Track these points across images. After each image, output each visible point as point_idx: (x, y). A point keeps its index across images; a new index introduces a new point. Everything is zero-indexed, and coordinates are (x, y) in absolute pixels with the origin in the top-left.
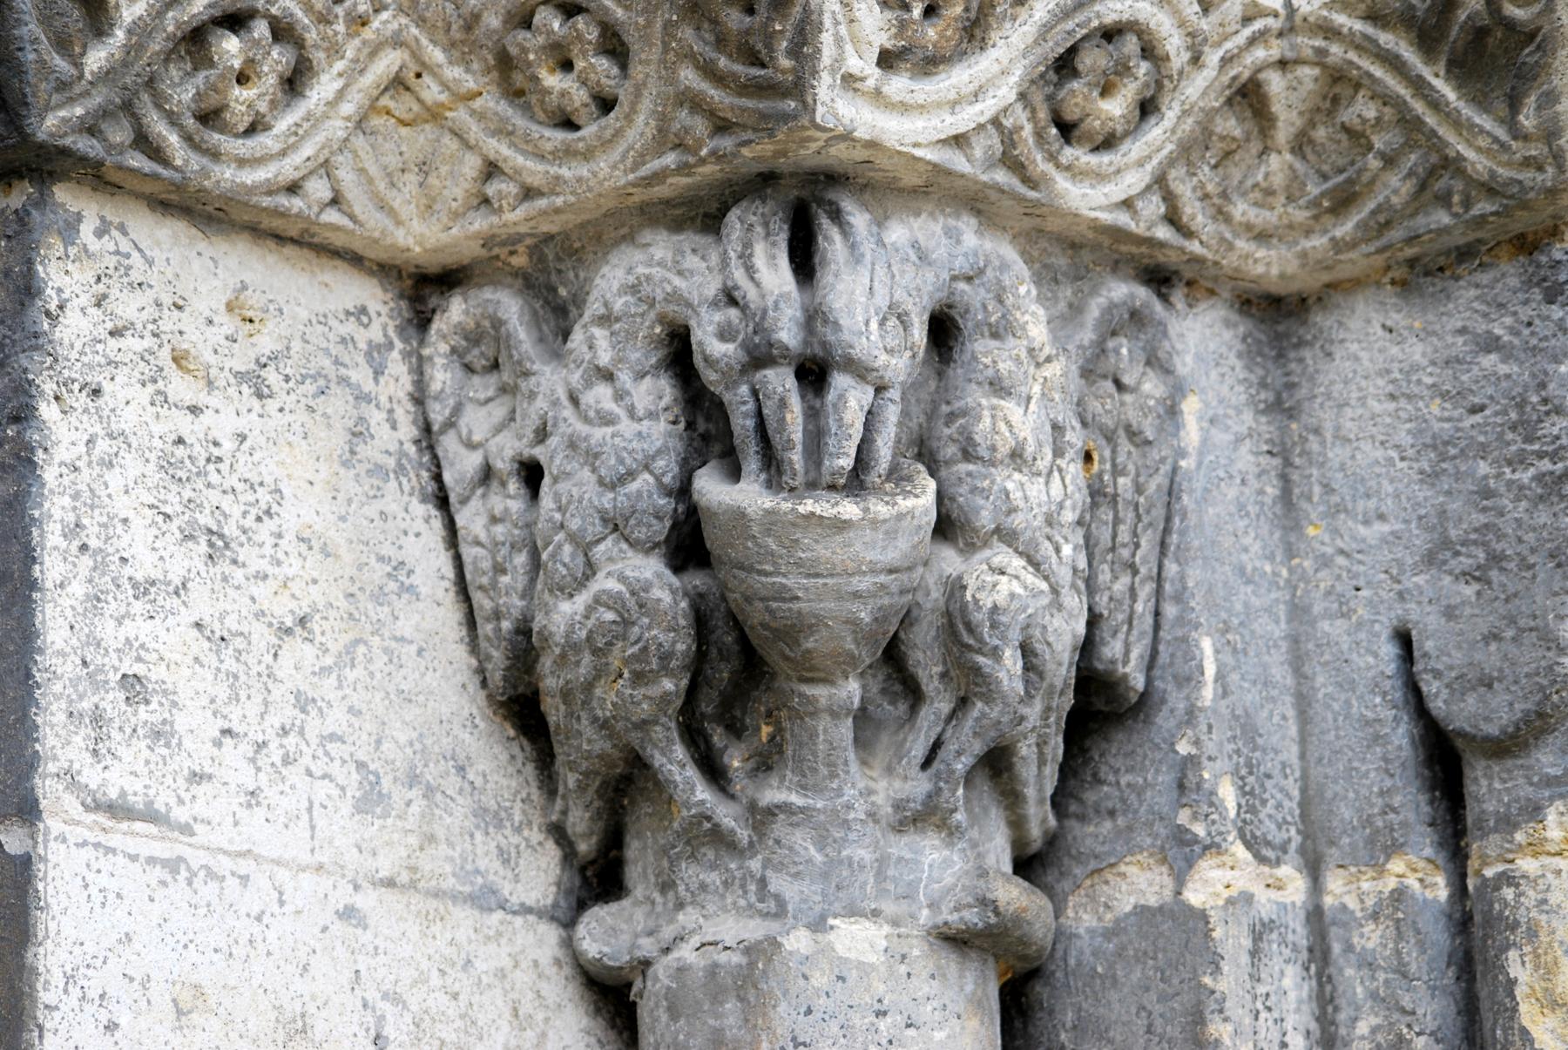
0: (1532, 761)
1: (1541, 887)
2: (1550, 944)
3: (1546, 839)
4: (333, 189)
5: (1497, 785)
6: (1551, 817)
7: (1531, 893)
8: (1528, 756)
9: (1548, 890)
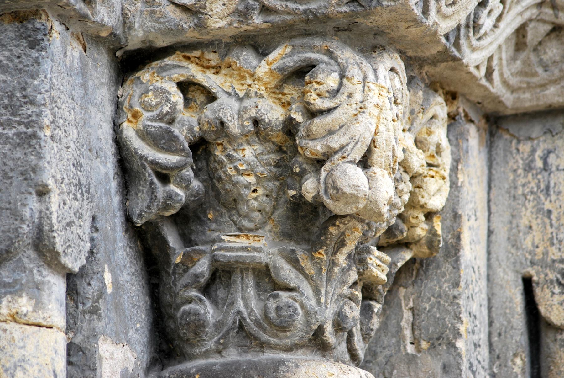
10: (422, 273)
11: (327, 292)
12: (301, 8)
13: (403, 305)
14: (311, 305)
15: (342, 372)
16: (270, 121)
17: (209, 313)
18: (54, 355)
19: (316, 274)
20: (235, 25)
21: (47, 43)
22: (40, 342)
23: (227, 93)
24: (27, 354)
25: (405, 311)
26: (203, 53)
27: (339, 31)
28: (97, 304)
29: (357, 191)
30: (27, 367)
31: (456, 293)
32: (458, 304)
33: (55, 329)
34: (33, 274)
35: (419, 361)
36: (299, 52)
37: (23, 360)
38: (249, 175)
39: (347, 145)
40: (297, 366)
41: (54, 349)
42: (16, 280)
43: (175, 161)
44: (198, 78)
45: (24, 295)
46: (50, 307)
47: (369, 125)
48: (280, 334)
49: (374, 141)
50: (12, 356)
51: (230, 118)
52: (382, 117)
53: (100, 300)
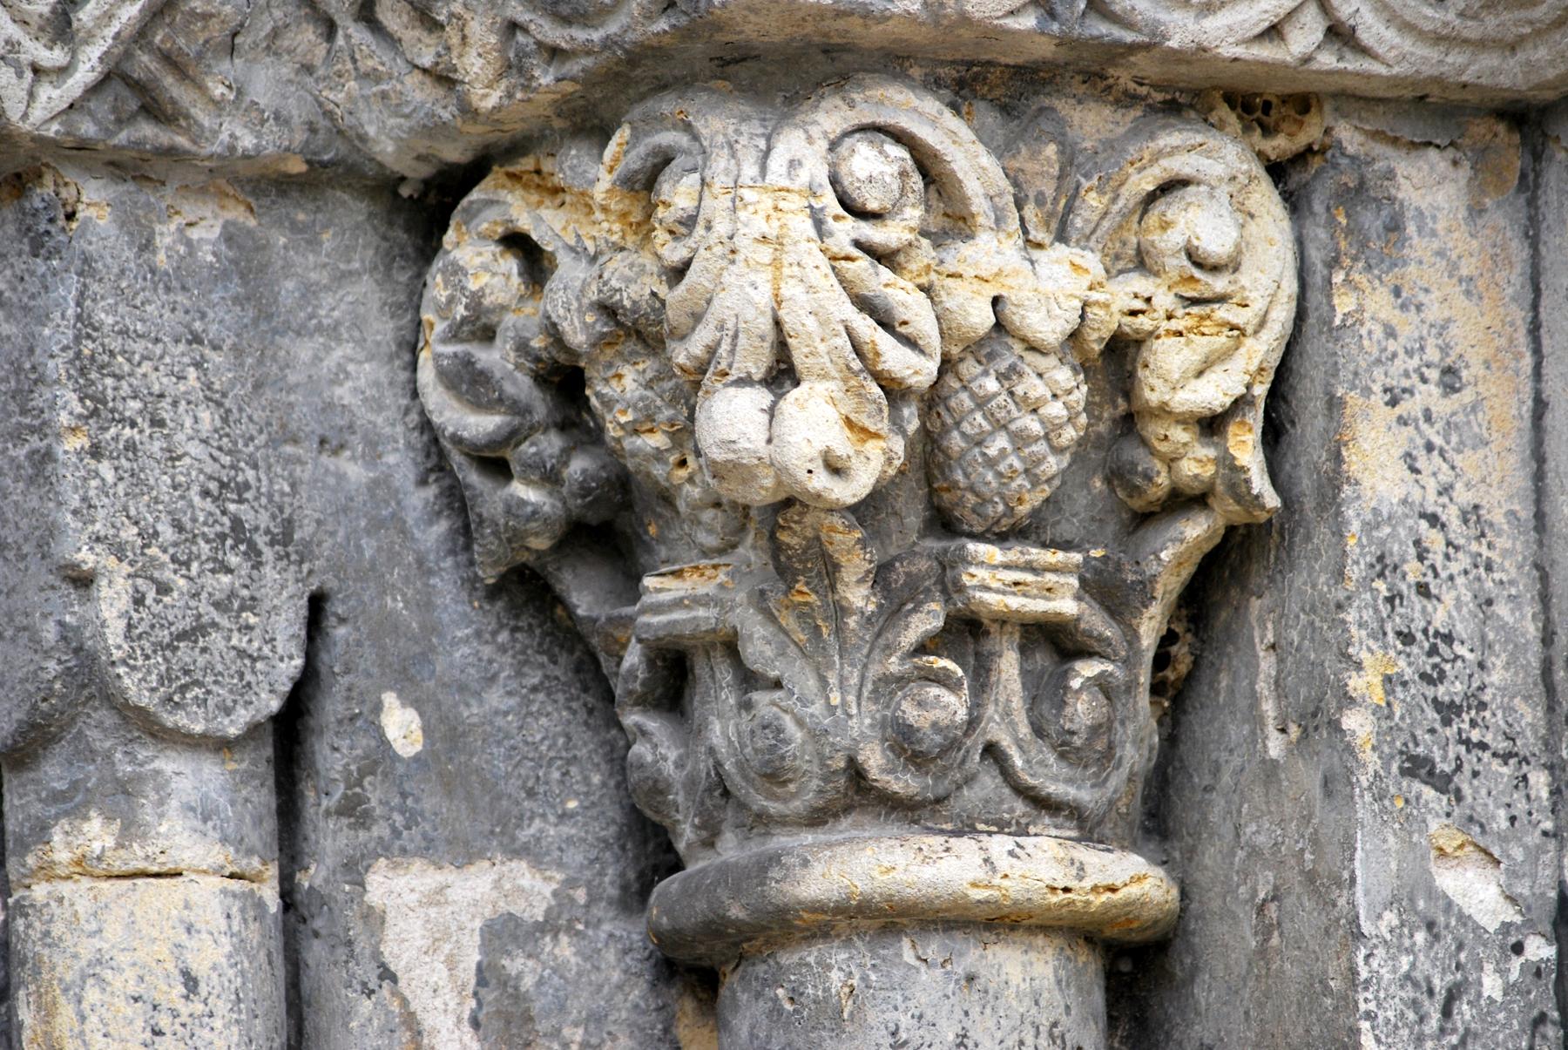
0: (41, 775)
1: (46, 917)
2: (50, 981)
3: (53, 862)
4: (1238, 246)
5: (16, 802)
6: (57, 837)
7: (37, 924)
8: (38, 768)
9: (51, 921)
10: (1284, 555)
11: (842, 680)
12: (596, 36)
13: (1257, 640)
14: (812, 715)
15: (920, 858)
16: (634, 302)
17: (665, 759)
18: (185, 936)
19: (809, 640)
20: (519, 95)
21: (62, 238)
22: (138, 913)
23: (572, 249)
24: (106, 946)
25: (1262, 654)
26: (538, 161)
27: (729, 63)
28: (358, 790)
29: (734, 451)
30: (108, 975)
31: (1341, 595)
32: (1344, 622)
33: (188, 876)
34: (113, 764)
35: (1283, 776)
36: (647, 134)
37: (99, 962)
38: (651, 431)
39: (719, 344)
40: (805, 863)
41: (182, 921)
42: (77, 781)
43: (491, 427)
44: (520, 224)
45: (93, 814)
46: (162, 829)
47: (749, 290)
48: (779, 791)
49: (778, 323)
50: (75, 956)
51: (561, 312)
52: (786, 263)
53: (367, 780)
